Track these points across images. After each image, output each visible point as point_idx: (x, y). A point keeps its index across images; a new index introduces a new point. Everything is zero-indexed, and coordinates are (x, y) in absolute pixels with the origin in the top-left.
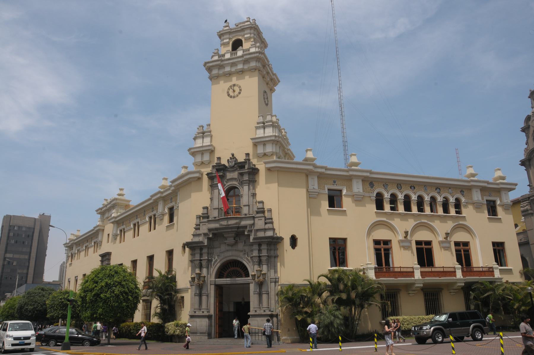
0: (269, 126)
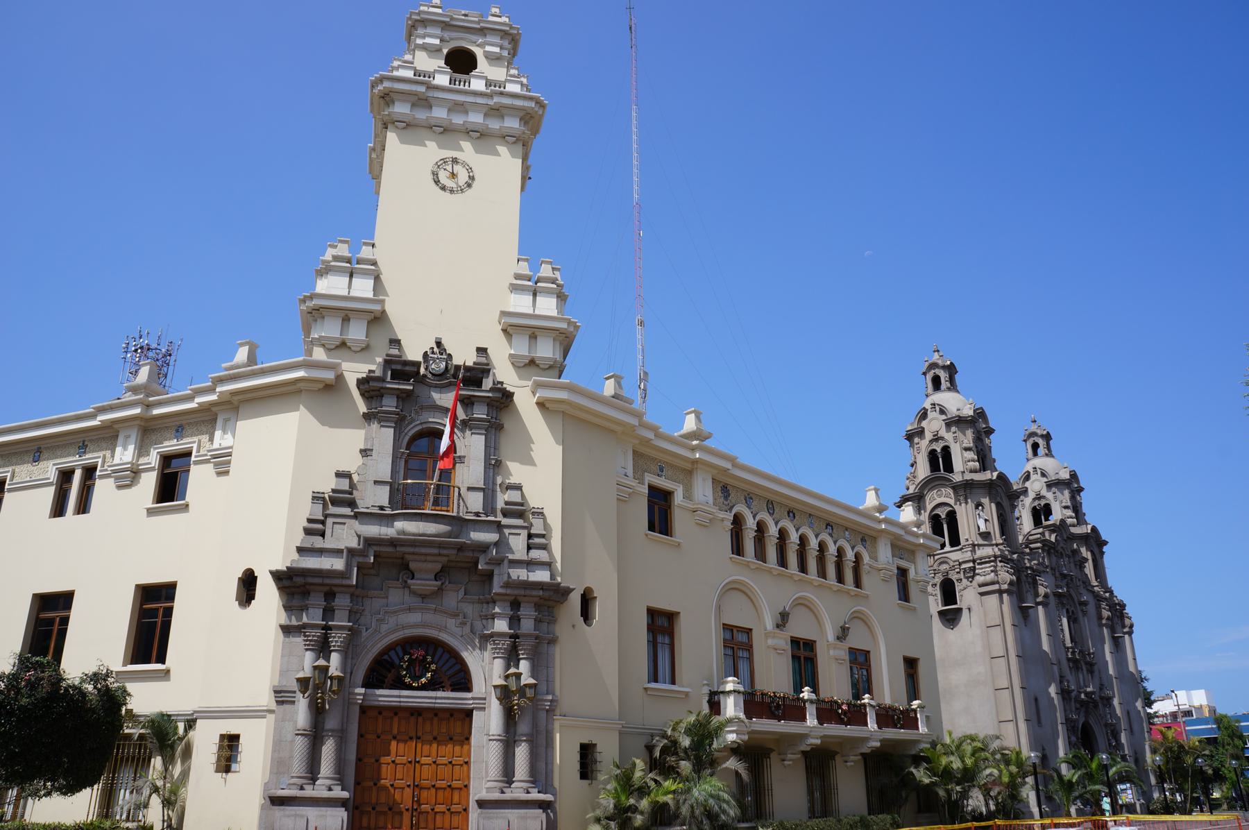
0: (548, 292)
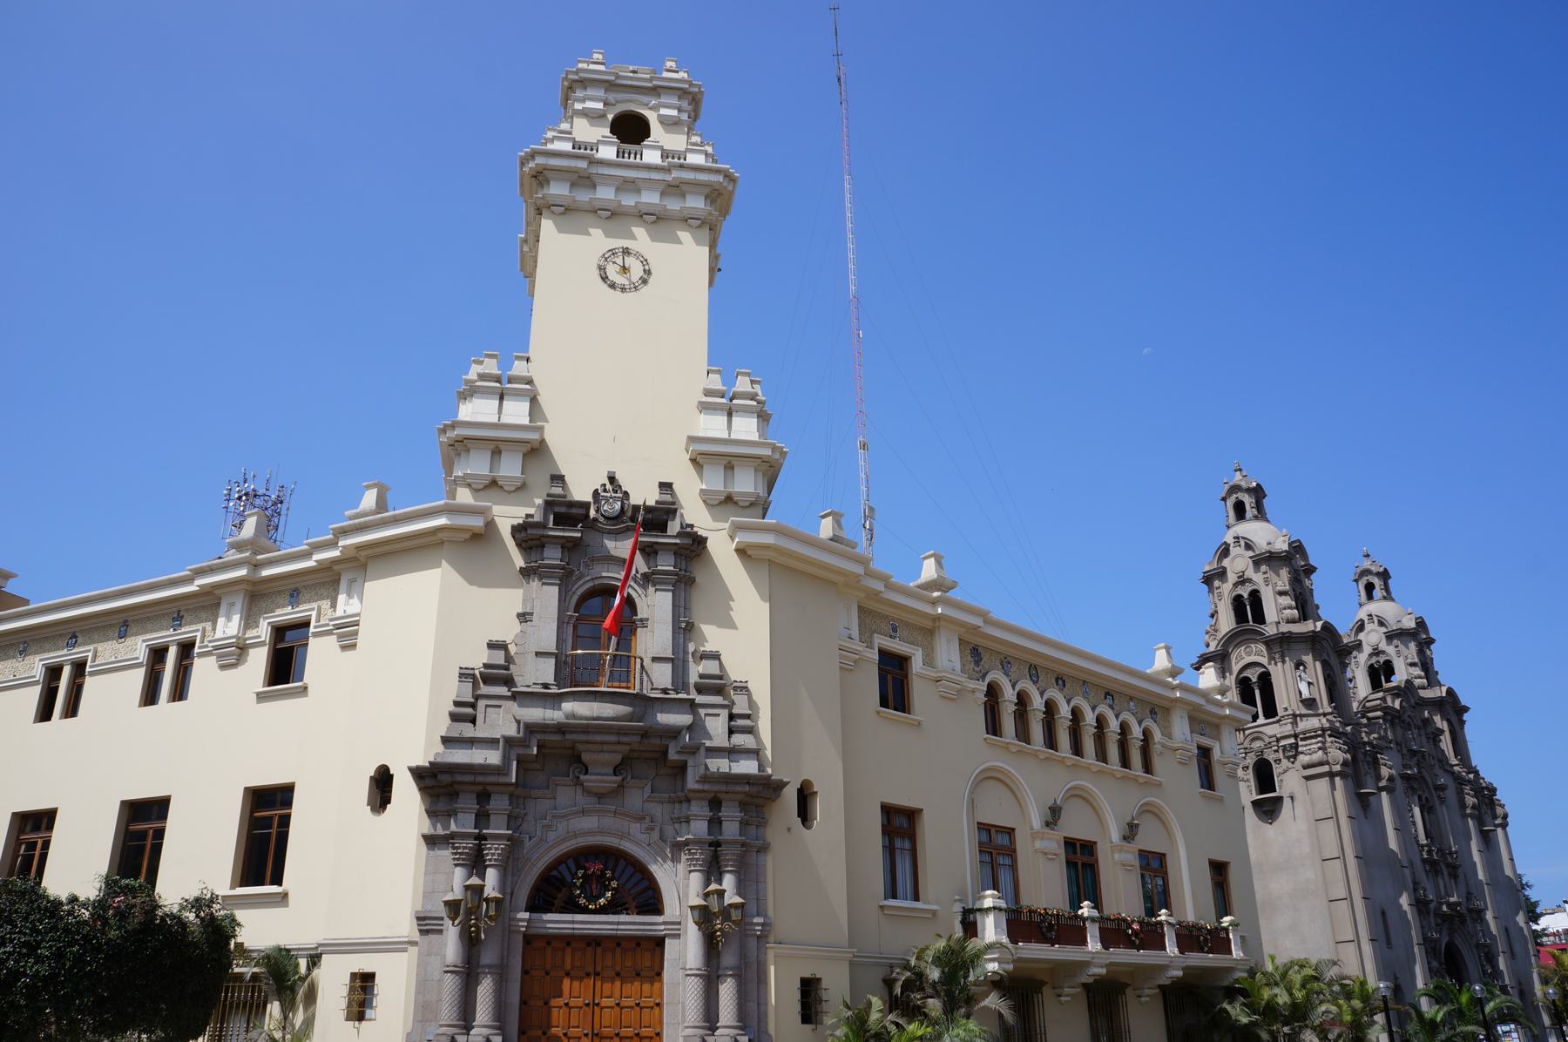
0: (746, 410)
